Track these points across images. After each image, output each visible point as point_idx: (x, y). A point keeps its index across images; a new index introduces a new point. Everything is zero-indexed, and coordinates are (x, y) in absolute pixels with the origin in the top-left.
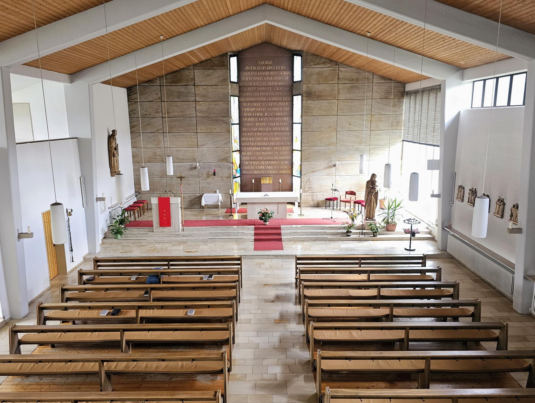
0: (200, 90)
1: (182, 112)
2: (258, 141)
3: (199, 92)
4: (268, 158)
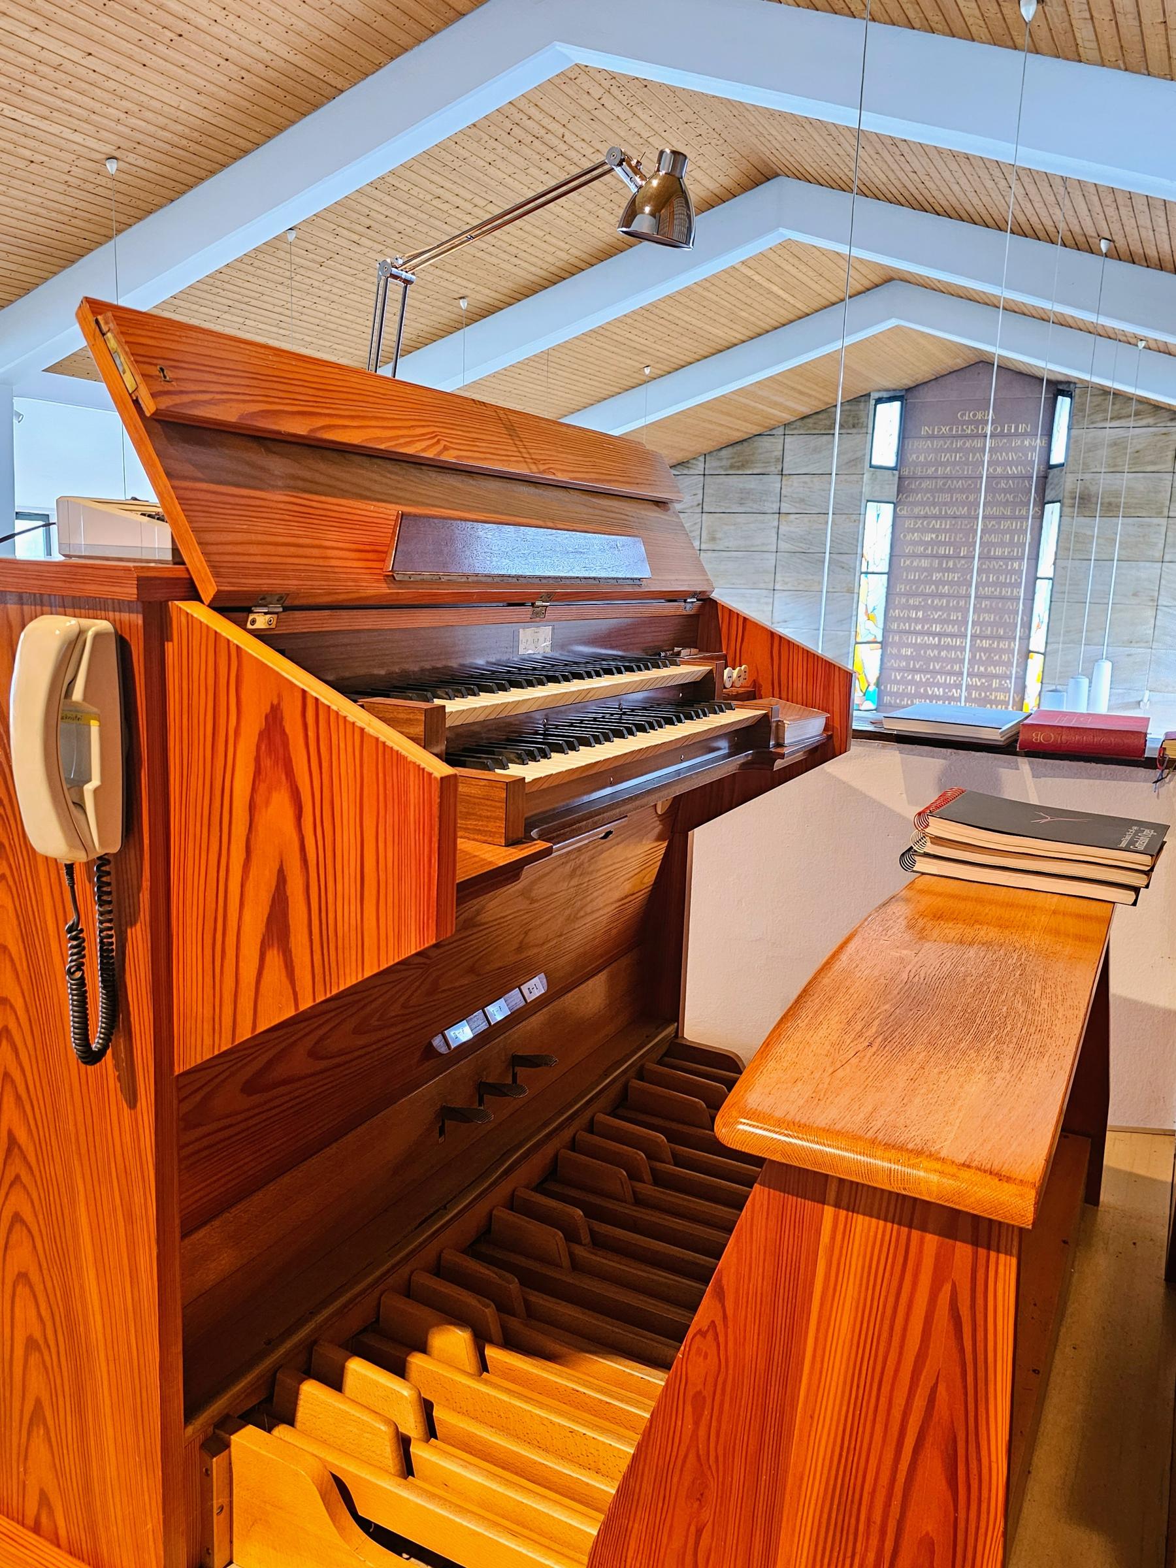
0: (793, 486)
3: (789, 490)
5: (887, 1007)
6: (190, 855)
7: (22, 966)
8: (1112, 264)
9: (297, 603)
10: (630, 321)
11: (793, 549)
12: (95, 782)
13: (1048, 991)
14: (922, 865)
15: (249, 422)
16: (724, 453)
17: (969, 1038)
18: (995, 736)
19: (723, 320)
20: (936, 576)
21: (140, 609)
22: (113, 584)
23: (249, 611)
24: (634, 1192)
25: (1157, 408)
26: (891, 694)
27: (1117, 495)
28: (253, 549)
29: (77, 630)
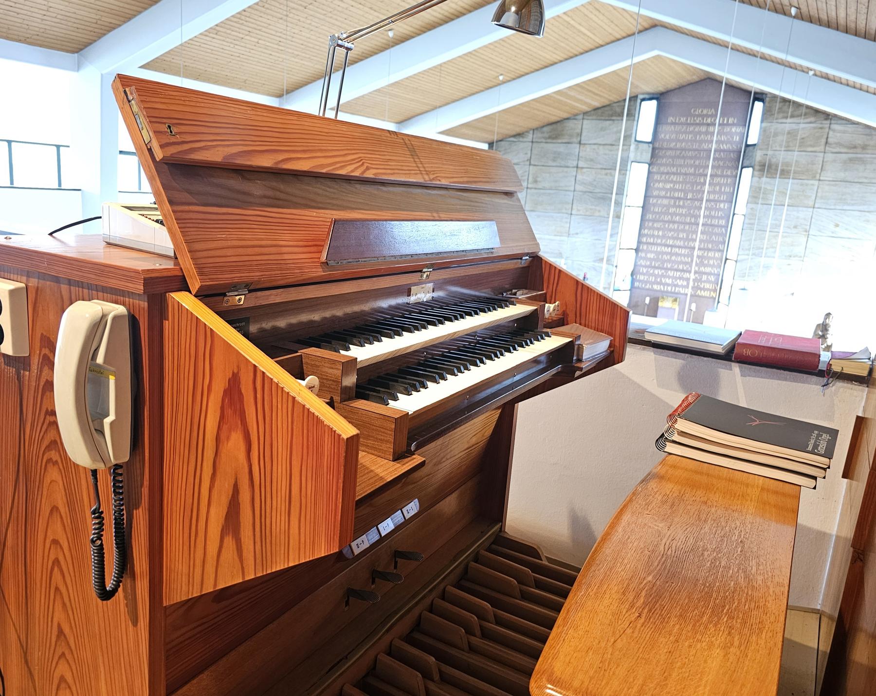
0: (587, 152)
1: (556, 181)
2: (669, 238)
4: (681, 267)
5: (650, 578)
6: (177, 464)
7: (67, 521)
8: (797, 22)
9: (258, 287)
10: (492, 47)
11: (584, 190)
12: (112, 417)
13: (761, 567)
14: (670, 448)
15: (230, 161)
16: (545, 129)
17: (709, 611)
18: (719, 350)
19: (550, 48)
20: (672, 210)
21: (146, 299)
22: (128, 281)
23: (224, 295)
24: (469, 643)
25: (817, 111)
26: (640, 281)
27: (788, 164)
28: (230, 252)
29: (101, 314)
